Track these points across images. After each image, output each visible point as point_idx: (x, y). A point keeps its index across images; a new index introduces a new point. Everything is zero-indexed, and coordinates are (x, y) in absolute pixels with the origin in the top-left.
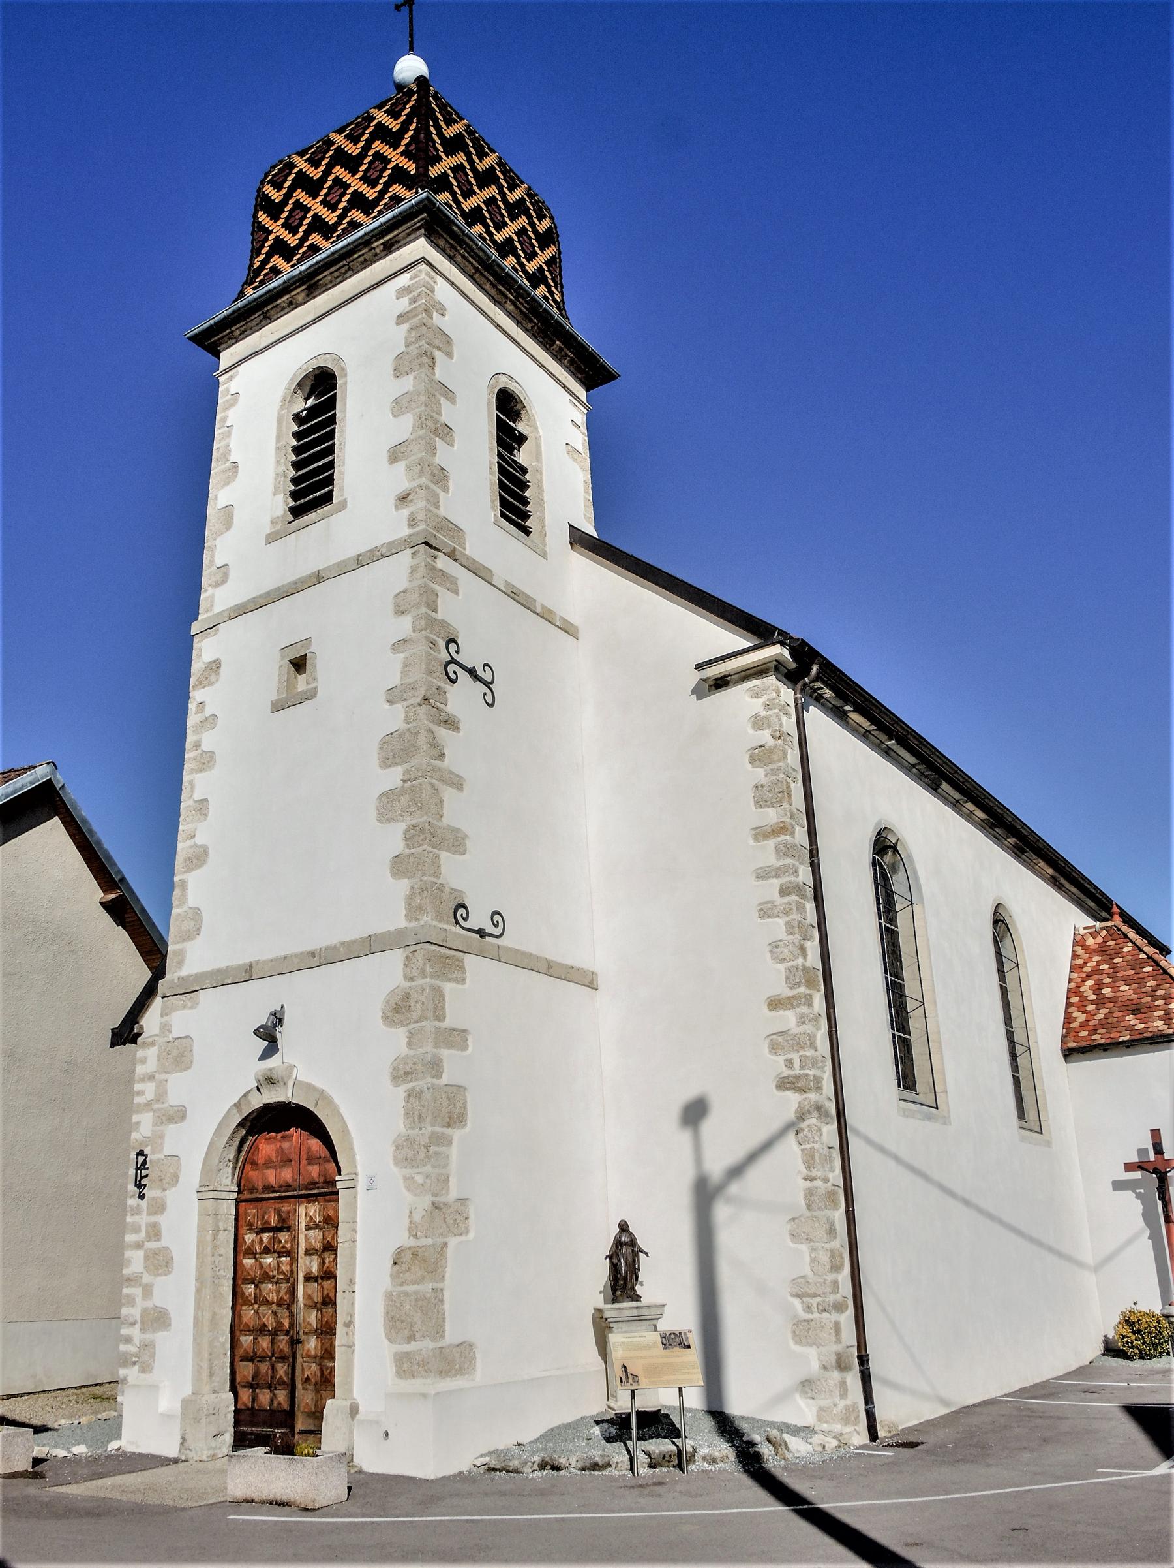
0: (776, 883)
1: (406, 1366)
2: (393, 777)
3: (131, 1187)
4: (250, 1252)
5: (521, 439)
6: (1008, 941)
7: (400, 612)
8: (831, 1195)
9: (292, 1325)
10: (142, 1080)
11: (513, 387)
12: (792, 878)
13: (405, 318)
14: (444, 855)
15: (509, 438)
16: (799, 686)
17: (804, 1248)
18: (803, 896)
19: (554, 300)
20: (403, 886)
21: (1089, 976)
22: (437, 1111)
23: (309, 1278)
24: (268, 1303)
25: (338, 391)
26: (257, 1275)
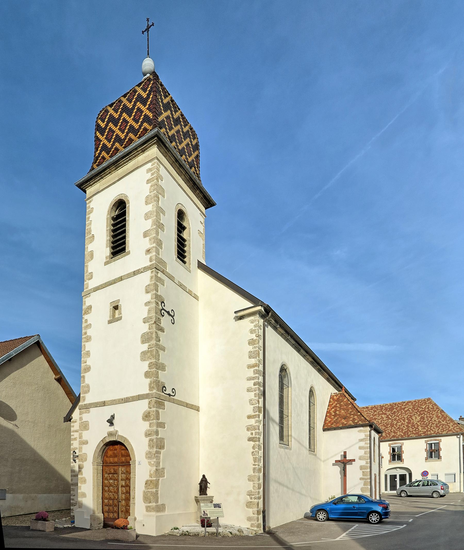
0: (253, 381)
1: (148, 509)
2: (145, 347)
3: (72, 460)
4: (106, 479)
5: (184, 228)
6: (313, 397)
7: (147, 292)
8: (259, 470)
9: (118, 498)
10: (73, 432)
11: (183, 209)
12: (257, 380)
13: (149, 181)
14: (160, 371)
15: (181, 228)
16: (265, 319)
17: (252, 483)
18: (260, 386)
19: (197, 173)
20: (148, 380)
21: (333, 408)
22: (158, 445)
23: (122, 486)
24: (111, 492)
25: (127, 209)
26: (108, 485)
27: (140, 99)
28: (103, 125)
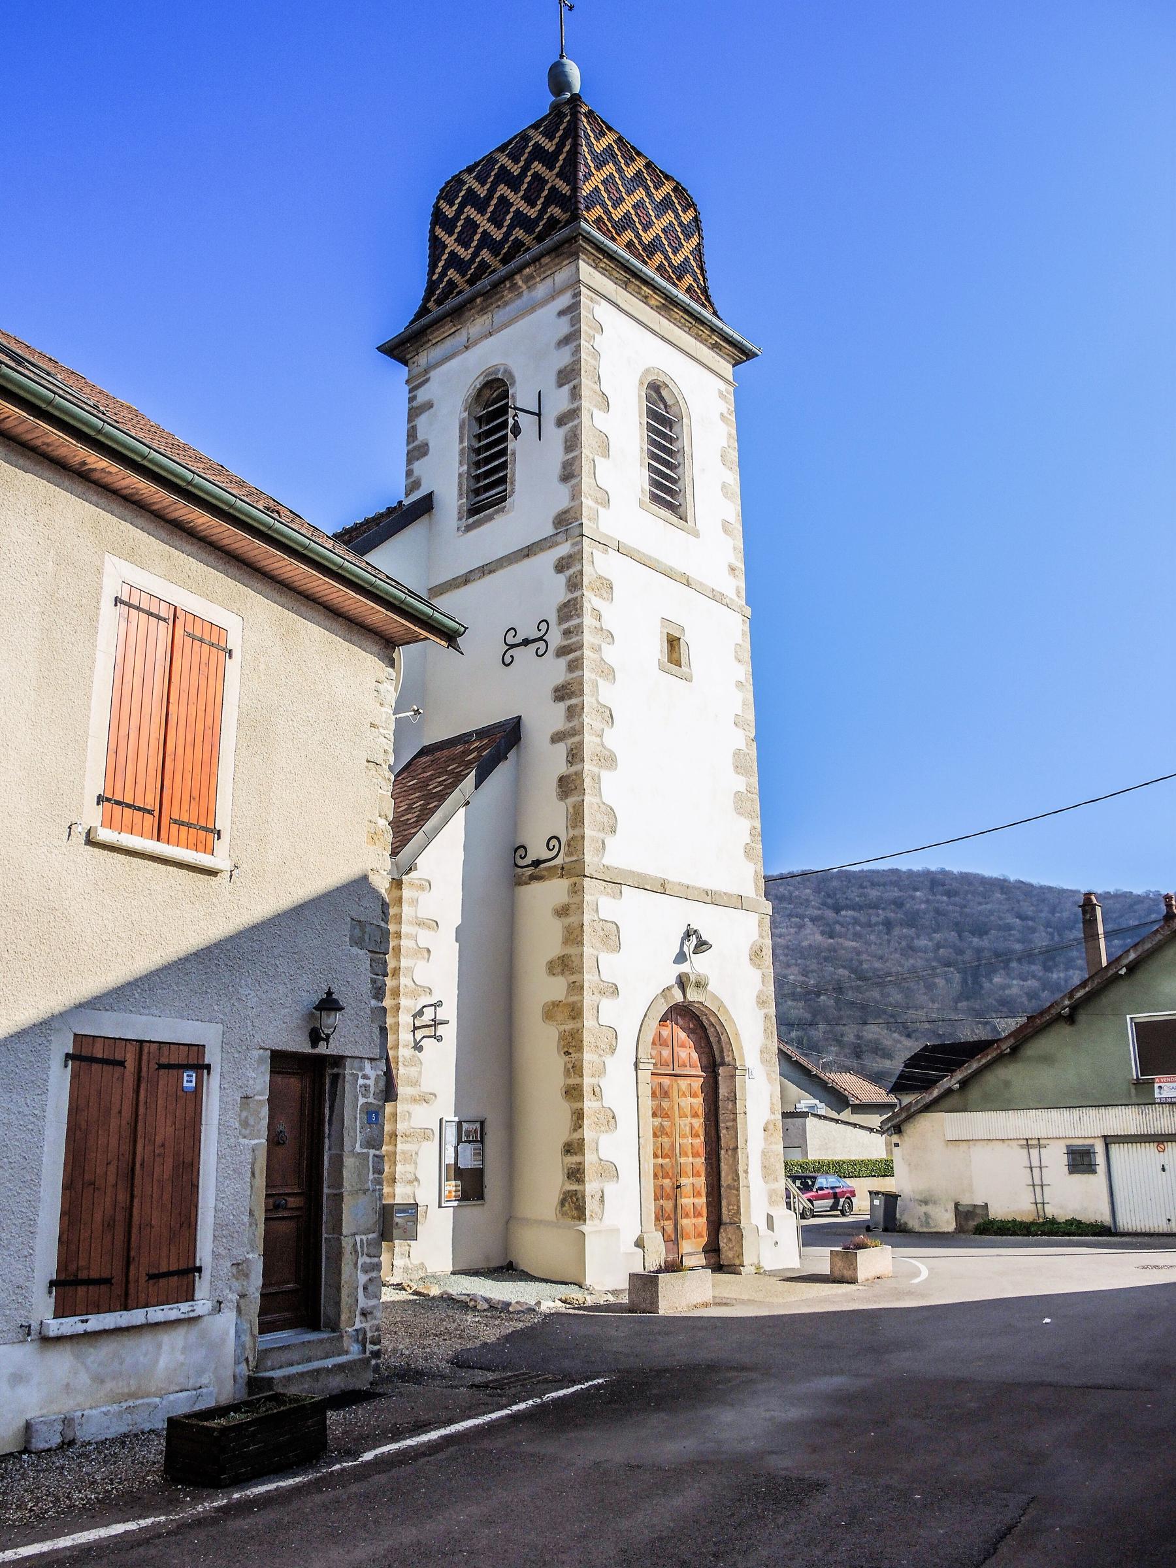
27: (539, 154)
28: (450, 212)
